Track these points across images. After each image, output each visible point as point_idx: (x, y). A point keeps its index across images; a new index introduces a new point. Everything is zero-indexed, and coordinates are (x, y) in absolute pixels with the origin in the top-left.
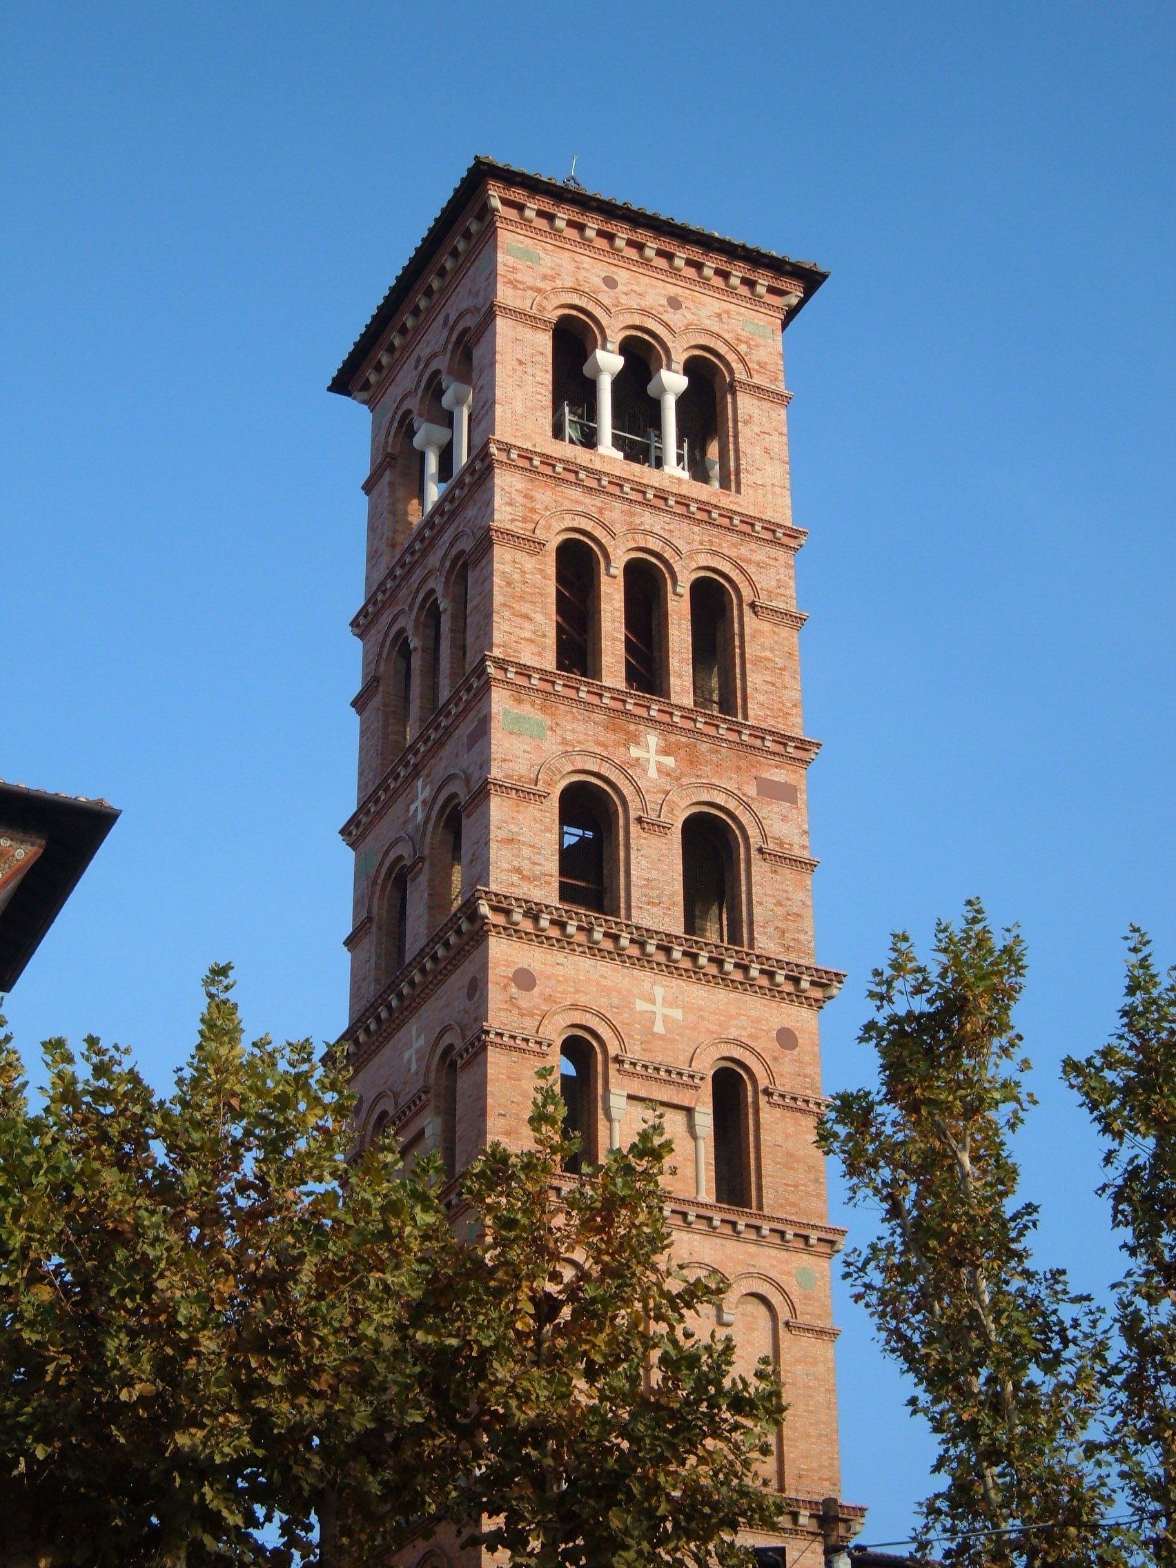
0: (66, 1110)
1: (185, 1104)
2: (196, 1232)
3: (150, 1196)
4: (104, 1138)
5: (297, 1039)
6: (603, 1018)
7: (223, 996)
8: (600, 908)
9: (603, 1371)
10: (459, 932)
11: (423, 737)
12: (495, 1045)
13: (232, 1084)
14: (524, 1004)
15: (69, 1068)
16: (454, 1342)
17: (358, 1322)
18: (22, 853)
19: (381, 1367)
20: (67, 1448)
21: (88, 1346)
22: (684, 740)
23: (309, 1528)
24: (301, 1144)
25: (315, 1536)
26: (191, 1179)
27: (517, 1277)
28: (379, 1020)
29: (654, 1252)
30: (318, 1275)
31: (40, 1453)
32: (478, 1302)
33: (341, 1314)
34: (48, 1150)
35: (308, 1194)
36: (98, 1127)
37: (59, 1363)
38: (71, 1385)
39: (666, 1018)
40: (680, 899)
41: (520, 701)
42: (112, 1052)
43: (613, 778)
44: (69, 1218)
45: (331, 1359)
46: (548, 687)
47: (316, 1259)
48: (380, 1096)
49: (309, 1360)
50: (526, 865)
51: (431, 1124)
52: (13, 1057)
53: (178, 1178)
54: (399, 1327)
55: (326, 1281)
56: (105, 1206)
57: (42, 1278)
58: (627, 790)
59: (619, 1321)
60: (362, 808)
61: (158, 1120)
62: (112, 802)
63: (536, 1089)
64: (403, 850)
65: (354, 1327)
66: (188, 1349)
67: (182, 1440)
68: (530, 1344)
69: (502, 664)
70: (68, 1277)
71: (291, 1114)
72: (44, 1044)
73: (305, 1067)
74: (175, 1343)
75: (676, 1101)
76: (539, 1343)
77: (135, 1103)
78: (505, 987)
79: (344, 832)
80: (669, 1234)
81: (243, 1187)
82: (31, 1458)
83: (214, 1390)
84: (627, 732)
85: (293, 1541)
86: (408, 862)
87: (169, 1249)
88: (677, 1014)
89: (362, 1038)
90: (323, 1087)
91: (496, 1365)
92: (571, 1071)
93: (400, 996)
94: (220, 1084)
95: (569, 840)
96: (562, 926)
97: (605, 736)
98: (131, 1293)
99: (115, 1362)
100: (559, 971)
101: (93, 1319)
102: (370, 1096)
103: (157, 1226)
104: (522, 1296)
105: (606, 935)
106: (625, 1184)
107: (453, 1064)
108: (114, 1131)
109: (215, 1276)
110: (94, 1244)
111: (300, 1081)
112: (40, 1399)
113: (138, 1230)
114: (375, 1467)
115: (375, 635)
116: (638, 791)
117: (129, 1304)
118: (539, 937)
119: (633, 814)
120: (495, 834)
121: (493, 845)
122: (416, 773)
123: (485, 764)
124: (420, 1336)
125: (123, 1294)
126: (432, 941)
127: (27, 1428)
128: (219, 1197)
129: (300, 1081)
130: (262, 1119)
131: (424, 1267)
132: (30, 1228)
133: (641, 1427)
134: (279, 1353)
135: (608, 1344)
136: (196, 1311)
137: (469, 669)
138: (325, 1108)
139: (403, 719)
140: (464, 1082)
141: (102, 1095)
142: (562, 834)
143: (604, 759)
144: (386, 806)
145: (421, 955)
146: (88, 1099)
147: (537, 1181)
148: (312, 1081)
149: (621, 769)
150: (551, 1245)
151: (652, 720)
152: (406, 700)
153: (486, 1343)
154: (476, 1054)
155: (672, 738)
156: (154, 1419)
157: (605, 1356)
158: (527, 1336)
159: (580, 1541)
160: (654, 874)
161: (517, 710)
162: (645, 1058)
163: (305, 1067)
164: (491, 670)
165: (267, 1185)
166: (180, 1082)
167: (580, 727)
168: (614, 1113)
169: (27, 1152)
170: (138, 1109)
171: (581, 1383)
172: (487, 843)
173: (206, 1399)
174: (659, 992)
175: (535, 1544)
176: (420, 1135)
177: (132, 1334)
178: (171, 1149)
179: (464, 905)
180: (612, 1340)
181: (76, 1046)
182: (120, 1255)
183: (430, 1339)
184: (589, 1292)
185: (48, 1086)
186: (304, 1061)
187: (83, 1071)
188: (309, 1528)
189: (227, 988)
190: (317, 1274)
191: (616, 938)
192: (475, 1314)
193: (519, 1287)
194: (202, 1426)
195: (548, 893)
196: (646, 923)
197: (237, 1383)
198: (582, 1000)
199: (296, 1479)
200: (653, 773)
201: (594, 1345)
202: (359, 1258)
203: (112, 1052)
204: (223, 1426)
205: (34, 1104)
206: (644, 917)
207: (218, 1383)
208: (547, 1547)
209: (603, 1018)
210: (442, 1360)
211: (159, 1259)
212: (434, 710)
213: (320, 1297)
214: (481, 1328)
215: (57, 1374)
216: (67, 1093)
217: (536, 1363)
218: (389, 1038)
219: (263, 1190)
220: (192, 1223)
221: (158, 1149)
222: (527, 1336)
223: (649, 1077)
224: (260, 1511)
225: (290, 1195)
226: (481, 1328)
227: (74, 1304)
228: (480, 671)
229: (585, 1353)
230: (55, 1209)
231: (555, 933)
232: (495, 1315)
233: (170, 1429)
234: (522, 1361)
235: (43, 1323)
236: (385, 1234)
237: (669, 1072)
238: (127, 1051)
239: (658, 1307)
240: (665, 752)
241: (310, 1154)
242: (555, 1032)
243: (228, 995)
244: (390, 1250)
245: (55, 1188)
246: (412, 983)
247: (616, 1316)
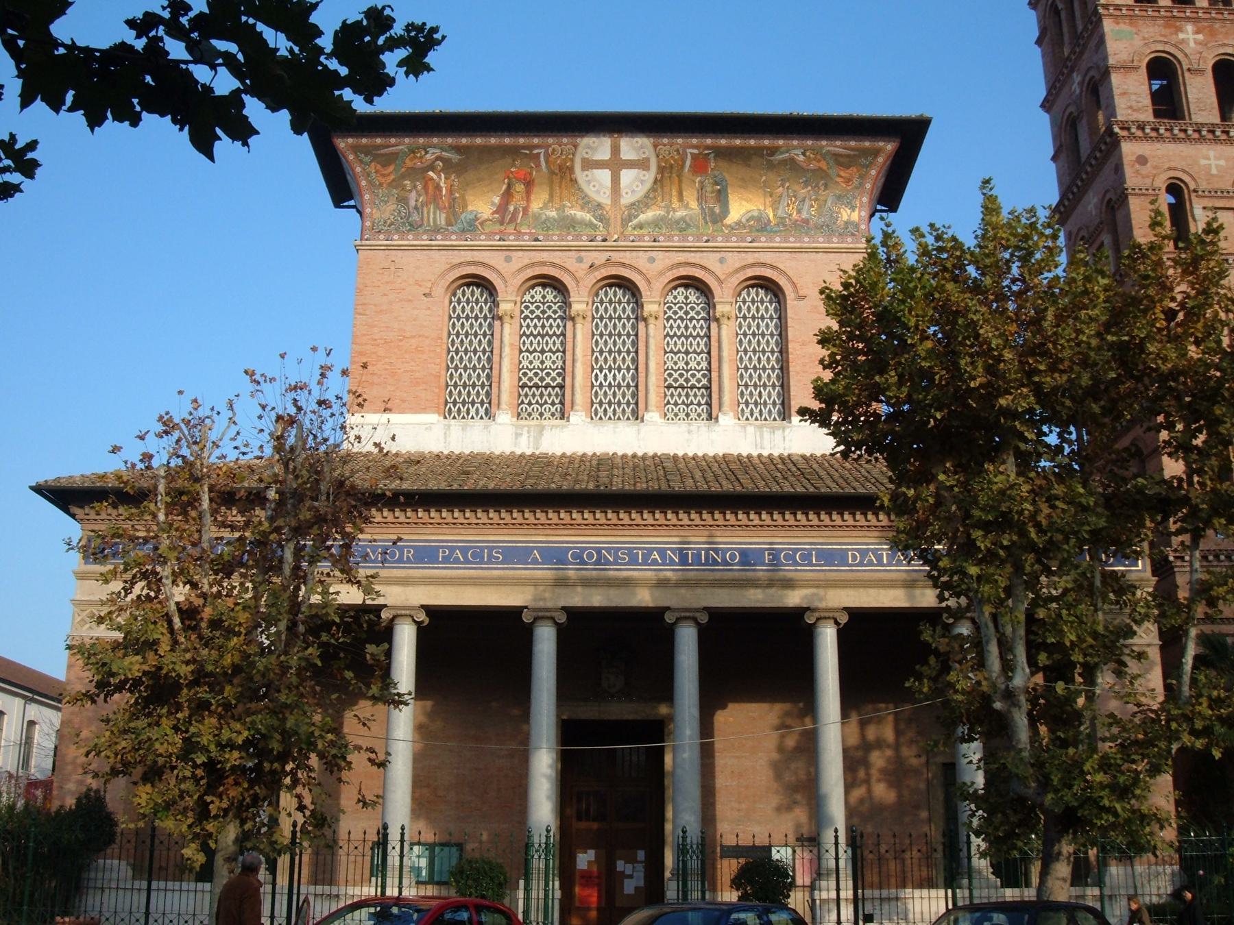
0: (926, 259)
1: (980, 246)
2: (995, 305)
3: (970, 292)
4: (945, 269)
5: (1028, 206)
6: (1185, 172)
7: (990, 193)
8: (1176, 119)
9: (1203, 340)
10: (1105, 143)
11: (1073, 52)
12: (1132, 195)
13: (1001, 234)
14: (1143, 172)
15: (924, 240)
16: (1126, 338)
17: (1078, 335)
18: (889, 147)
19: (1092, 354)
20: (950, 412)
21: (952, 365)
22: (1206, 24)
23: (1070, 433)
24: (1038, 256)
25: (1074, 437)
26: (988, 281)
27: (1153, 302)
28: (1073, 193)
29: (1222, 279)
30: (1055, 316)
31: (938, 416)
32: (1136, 317)
33: (1069, 332)
34: (920, 279)
35: (1045, 279)
36: (942, 265)
37: (940, 375)
38: (948, 384)
39: (1217, 166)
40: (1216, 105)
41: (1118, 23)
42: (942, 229)
43: (1172, 51)
44: (935, 308)
45: (1067, 354)
46: (1131, 13)
47: (1053, 309)
48: (1080, 229)
49: (1057, 356)
50: (1134, 104)
51: (1106, 239)
52: (897, 240)
53: (982, 281)
54: (1099, 335)
55: (1060, 319)
56: (950, 300)
57: (928, 338)
58: (1180, 56)
59: (1208, 315)
60: (1049, 93)
61: (968, 256)
62: (927, 114)
63: (1151, 211)
64: (1072, 109)
65: (1077, 338)
66: (999, 359)
67: (1003, 402)
68: (1165, 333)
69: (1106, 7)
70: (940, 336)
71: (1030, 243)
72: (910, 231)
73: (1034, 219)
74: (993, 357)
75: (1227, 206)
76: (1169, 331)
77: (957, 250)
78: (1133, 166)
79: (1042, 106)
80: (1227, 270)
81: (1014, 281)
82: (935, 419)
83: (1014, 376)
84: (1176, 27)
85: (1063, 440)
86: (1076, 114)
87: (983, 315)
88: (1222, 163)
89: (1066, 203)
90: (1045, 227)
91: (1148, 345)
92: (1172, 200)
93: (1082, 180)
94: (995, 235)
95: (1155, 87)
96: (1157, 130)
97: (1164, 31)
98: (968, 338)
99: (966, 370)
100: (1159, 152)
101: (954, 353)
102: (1075, 230)
103: (975, 305)
104: (1157, 311)
105: (1180, 130)
106: (1202, 249)
107: (1113, 208)
108: (949, 265)
109: (1007, 324)
110: (948, 318)
111: (1033, 226)
112: (935, 391)
113: (967, 309)
114: (1096, 400)
115: (1041, 7)
116: (1186, 55)
117: (968, 343)
118: (1147, 138)
119: (1185, 67)
120: (1116, 91)
121: (1116, 97)
122: (1072, 71)
123: (1105, 58)
124: (1109, 338)
125: (964, 338)
126: (1093, 150)
127: (931, 406)
128: (1004, 287)
129: (1033, 226)
130: (1018, 248)
131: (1107, 305)
132: (917, 316)
133: (1225, 364)
134: (1041, 355)
135: (1204, 327)
136: (1000, 341)
137: (1090, 12)
138: (1047, 237)
139: (1061, 44)
140: (1120, 215)
141: (940, 250)
142: (1150, 85)
143: (1166, 43)
144: (1061, 89)
145: (1089, 157)
146: (934, 252)
147: (1156, 255)
148: (1038, 226)
149: (1175, 46)
150: (1168, 284)
151: (1188, 18)
152: (1062, 35)
153: (1142, 336)
154: (1123, 201)
155: (1200, 25)
156: (989, 394)
157: (1202, 333)
158: (1163, 329)
159: (1202, 422)
160: (1201, 95)
161: (1117, 28)
162: (1209, 187)
163: (1034, 219)
164: (1101, 10)
165: (1024, 278)
166: (976, 237)
167: (1151, 29)
168: (1197, 217)
169: (910, 282)
170: (958, 253)
171: (1192, 348)
172: (1112, 97)
173: (1011, 381)
174: (1212, 154)
175: (1180, 427)
176: (1102, 244)
177: (971, 355)
178: (977, 269)
179: (1106, 129)
180: (1205, 326)
181: (925, 229)
182: (960, 321)
183: (1115, 338)
184: (1190, 303)
185: (915, 250)
186: (1033, 216)
187: (930, 240)
188: (1070, 433)
189: (991, 189)
190: (1055, 315)
191: (1185, 131)
192: (1135, 323)
193: (1155, 307)
194: (1011, 394)
195: (1148, 116)
196: (1200, 120)
197: (1025, 371)
198: (1173, 164)
199: (1059, 412)
200: (1192, 44)
201: (1196, 329)
202: (1075, 305)
203: (942, 229)
204: (1020, 394)
205: (911, 259)
206: (1198, 118)
207: (1016, 373)
208: (1187, 426)
209: (1185, 172)
210: (1121, 347)
211: (979, 320)
212: (1076, 37)
213: (1058, 326)
214: (1139, 329)
215: (941, 379)
216: (925, 252)
217: (1169, 342)
218: (1079, 200)
219: (1023, 281)
220: (992, 301)
221: (971, 270)
222: (1163, 329)
223: (1213, 197)
224: (1045, 429)
225: (1036, 281)
226: (1139, 329)
227: (944, 347)
228: (1096, 12)
229: (1192, 334)
230: (928, 305)
231: (1154, 134)
232: (1144, 322)
233: (997, 397)
234: (1161, 342)
235: (930, 357)
236: (1086, 292)
237: (1222, 192)
238: (949, 227)
239: (1226, 306)
240: (1197, 32)
241: (1043, 260)
242: (1161, 182)
243: (992, 192)
244: (1089, 299)
245: (926, 296)
246: (1087, 173)
247: (1205, 314)
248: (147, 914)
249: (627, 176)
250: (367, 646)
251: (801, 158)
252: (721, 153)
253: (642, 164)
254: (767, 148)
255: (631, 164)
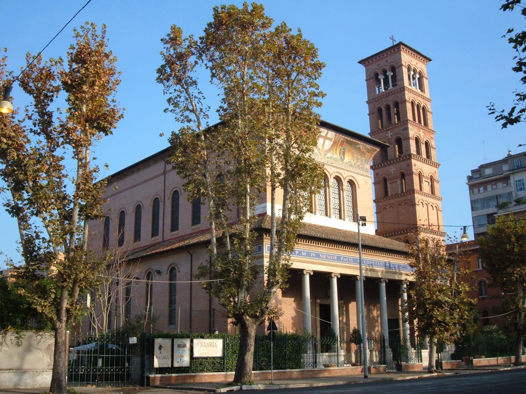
9: (58, 169)
248: (338, 362)
249: (327, 141)
250: (415, 280)
251: (362, 148)
252: (348, 142)
253: (330, 139)
254: (356, 143)
255: (329, 139)
